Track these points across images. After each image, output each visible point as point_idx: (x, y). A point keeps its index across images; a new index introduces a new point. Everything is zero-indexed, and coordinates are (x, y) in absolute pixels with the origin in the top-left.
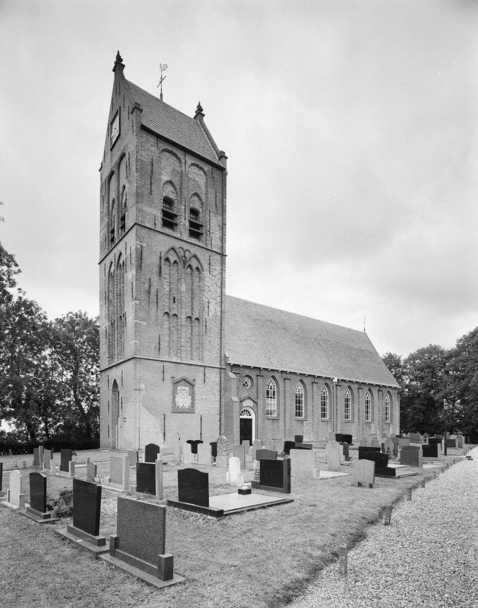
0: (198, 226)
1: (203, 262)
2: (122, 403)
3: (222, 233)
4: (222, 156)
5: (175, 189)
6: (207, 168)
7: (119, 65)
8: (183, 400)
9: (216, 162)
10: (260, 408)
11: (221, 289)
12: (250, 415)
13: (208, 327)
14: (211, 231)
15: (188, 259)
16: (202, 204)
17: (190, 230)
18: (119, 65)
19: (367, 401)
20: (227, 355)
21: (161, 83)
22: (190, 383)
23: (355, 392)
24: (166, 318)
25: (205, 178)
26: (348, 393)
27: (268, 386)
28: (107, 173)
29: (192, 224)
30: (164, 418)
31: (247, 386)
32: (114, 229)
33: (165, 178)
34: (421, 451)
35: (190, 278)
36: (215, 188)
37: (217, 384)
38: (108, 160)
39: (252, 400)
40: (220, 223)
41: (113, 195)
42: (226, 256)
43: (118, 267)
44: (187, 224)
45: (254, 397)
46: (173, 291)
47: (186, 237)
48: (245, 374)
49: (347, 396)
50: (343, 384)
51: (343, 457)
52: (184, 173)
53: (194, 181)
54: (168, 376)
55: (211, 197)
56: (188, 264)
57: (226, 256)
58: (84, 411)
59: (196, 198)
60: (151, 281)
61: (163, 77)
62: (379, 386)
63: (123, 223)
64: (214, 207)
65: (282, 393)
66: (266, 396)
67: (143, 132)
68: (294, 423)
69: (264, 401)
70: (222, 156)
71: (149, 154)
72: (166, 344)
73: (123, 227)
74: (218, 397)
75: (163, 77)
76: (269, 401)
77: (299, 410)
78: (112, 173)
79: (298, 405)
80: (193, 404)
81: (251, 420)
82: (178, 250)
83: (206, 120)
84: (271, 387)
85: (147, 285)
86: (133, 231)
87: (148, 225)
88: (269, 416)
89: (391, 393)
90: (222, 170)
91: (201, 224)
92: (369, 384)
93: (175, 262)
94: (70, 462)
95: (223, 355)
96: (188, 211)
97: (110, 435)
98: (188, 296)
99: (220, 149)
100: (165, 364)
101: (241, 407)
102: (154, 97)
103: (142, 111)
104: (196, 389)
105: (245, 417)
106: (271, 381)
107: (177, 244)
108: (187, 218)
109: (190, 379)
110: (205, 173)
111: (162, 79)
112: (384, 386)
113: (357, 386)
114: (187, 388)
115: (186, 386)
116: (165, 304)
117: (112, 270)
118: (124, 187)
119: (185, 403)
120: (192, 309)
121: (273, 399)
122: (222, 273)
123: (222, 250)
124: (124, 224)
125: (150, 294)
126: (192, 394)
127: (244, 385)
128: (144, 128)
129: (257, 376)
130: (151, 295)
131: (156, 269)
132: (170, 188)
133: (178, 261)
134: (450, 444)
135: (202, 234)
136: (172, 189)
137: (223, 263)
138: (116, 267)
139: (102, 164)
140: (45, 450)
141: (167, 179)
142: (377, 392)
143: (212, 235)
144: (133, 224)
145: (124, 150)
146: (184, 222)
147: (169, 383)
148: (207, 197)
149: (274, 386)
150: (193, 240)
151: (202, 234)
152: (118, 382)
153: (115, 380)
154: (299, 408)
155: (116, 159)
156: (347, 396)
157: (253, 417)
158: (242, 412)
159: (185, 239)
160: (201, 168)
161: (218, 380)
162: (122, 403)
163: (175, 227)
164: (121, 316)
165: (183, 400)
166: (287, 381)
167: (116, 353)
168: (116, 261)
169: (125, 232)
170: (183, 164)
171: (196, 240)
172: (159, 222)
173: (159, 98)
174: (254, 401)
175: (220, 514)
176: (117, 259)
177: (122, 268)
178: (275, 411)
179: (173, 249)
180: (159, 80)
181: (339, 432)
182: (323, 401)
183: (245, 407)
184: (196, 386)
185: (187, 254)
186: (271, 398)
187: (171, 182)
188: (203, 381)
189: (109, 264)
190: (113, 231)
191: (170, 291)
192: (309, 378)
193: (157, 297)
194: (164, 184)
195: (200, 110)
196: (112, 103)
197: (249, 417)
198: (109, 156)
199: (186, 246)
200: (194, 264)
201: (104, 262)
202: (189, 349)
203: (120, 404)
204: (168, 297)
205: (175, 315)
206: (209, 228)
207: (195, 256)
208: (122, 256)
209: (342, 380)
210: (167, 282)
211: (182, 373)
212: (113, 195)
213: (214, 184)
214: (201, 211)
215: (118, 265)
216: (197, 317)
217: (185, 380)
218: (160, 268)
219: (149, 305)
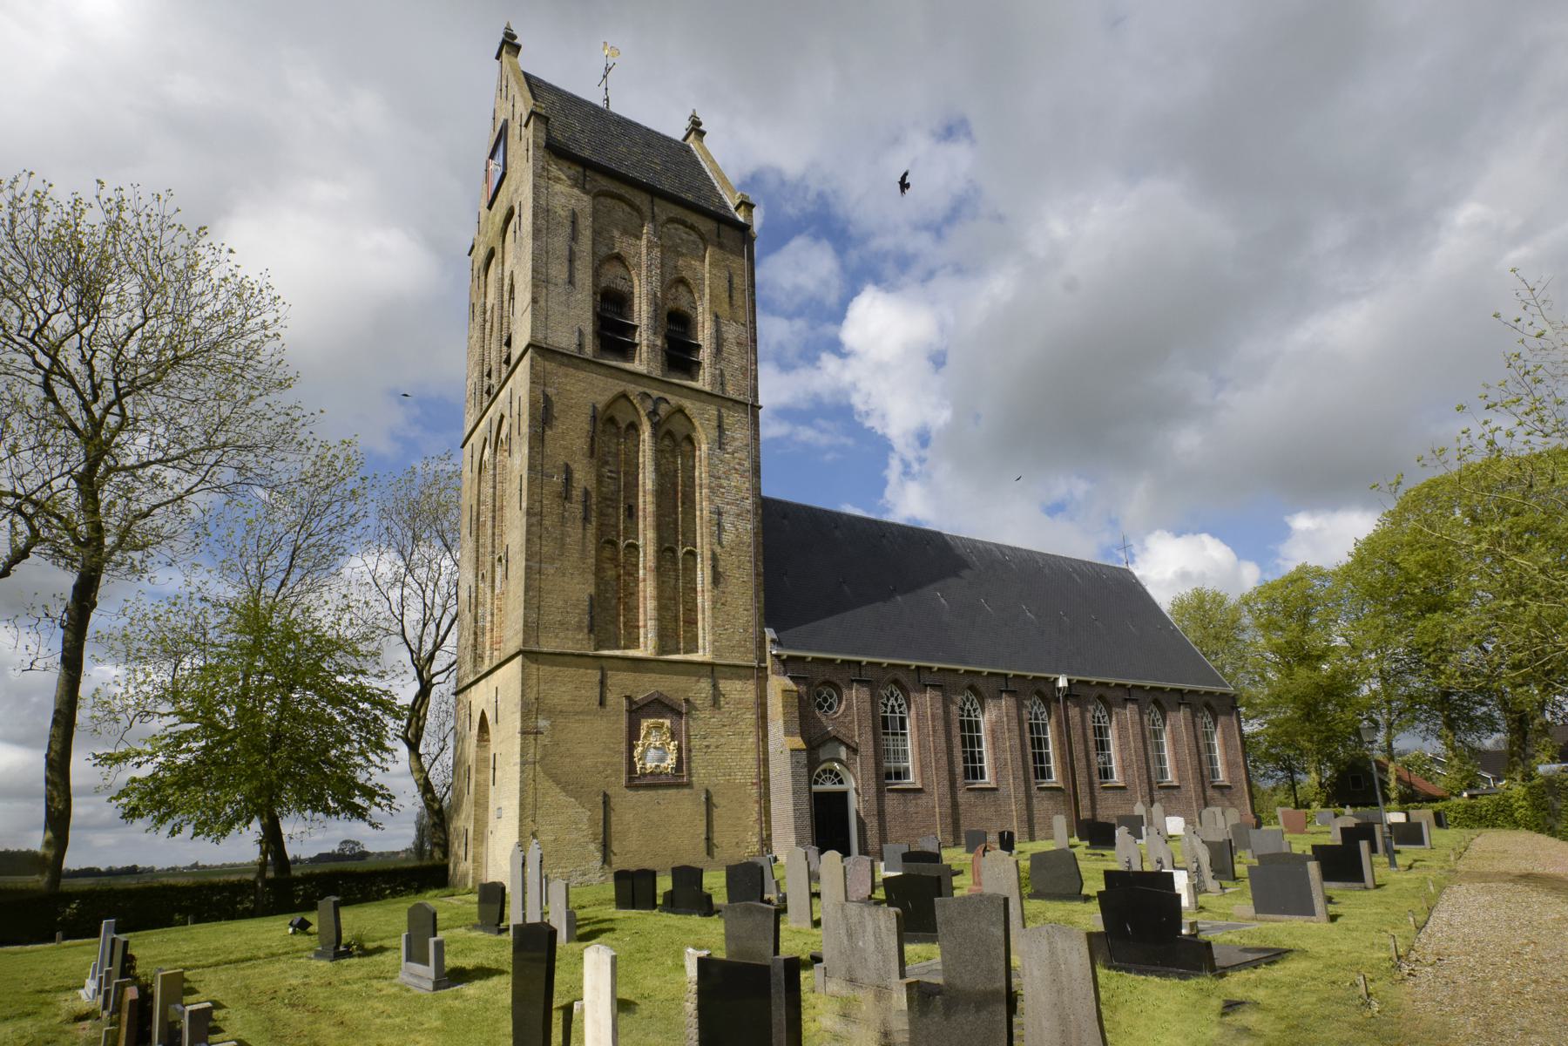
2: (494, 769)
12: (841, 782)
21: (605, 76)
27: (886, 706)
50: (1084, 691)
51: (686, 791)
56: (664, 429)
58: (1180, 927)
61: (610, 65)
64: (726, 306)
75: (610, 65)
81: (843, 796)
84: (893, 706)
86: (526, 361)
92: (1152, 688)
94: (432, 940)
105: (829, 787)
111: (608, 70)
140: (1102, 973)
160: (692, 227)
162: (494, 769)
180: (603, 72)
197: (838, 787)
219: (563, 525)
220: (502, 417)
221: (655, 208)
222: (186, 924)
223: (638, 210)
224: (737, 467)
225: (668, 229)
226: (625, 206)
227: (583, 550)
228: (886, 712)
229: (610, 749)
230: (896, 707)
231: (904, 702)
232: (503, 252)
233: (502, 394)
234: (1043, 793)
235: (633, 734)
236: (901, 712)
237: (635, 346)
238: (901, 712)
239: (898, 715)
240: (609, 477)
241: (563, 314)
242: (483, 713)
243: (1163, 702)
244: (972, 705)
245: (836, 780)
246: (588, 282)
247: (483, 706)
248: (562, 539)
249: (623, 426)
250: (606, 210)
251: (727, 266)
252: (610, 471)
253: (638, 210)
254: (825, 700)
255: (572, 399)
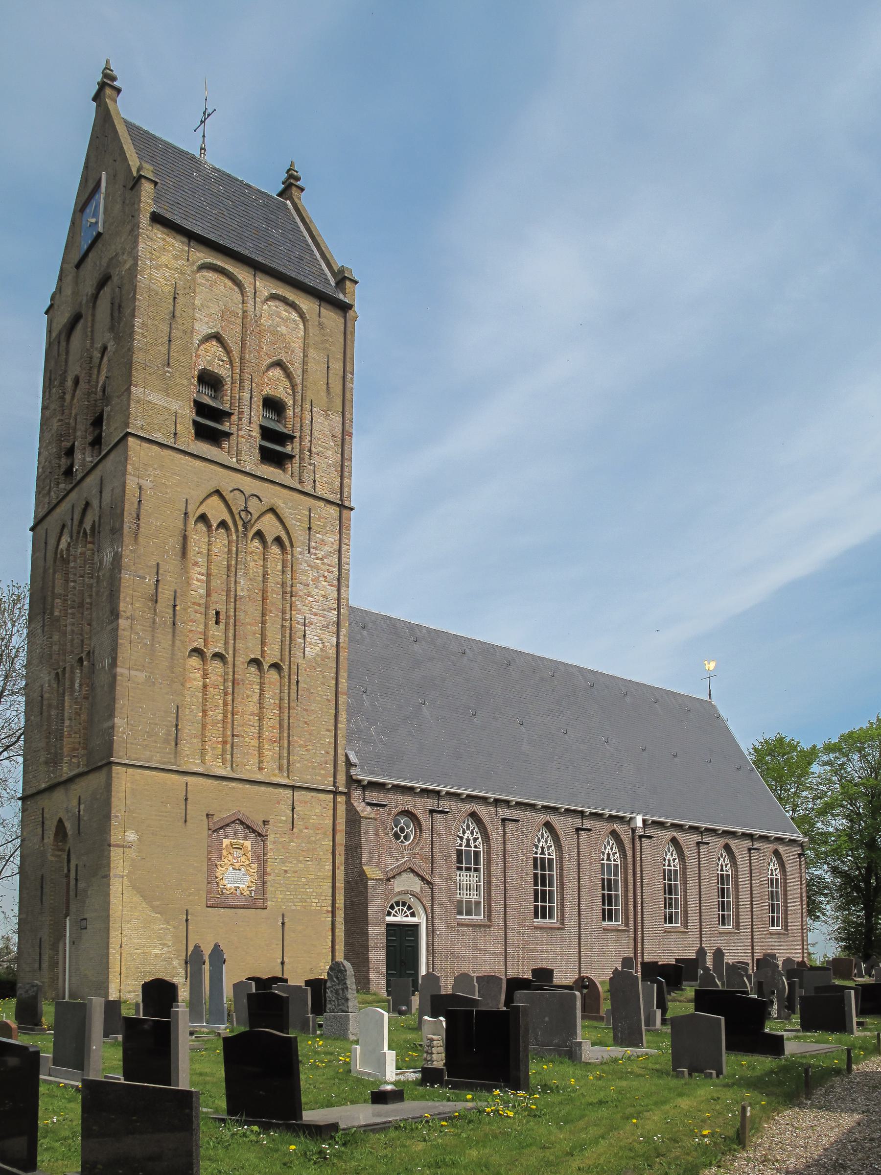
0: (283, 438)
1: (291, 522)
2: (76, 880)
3: (342, 455)
4: (342, 279)
5: (228, 351)
11: (339, 590)
12: (413, 915)
14: (313, 450)
15: (255, 516)
16: (293, 387)
17: (262, 449)
19: (722, 875)
21: (203, 122)
22: (254, 831)
23: (690, 853)
25: (301, 326)
26: (546, 842)
27: (461, 838)
28: (63, 318)
29: (267, 433)
30: (187, 920)
31: (406, 838)
33: (203, 328)
36: (325, 349)
37: (325, 833)
38: (68, 291)
39: (418, 875)
40: (338, 431)
42: (352, 509)
43: (78, 537)
44: (256, 433)
45: (424, 868)
46: (214, 597)
47: (251, 460)
48: (400, 808)
49: (722, 870)
52: (251, 313)
53: (275, 333)
54: (196, 813)
55: (316, 369)
57: (352, 509)
59: (277, 372)
60: (161, 572)
61: (209, 111)
63: (97, 432)
64: (323, 394)
65: (497, 859)
66: (455, 865)
69: (450, 876)
71: (167, 275)
72: (196, 729)
73: (97, 442)
74: (329, 867)
75: (209, 111)
76: (464, 878)
78: (77, 318)
79: (606, 892)
80: (262, 884)
81: (415, 927)
82: (229, 497)
83: (305, 200)
84: (468, 840)
85: (150, 580)
87: (158, 437)
91: (291, 433)
96: (258, 402)
97: (45, 965)
99: (339, 262)
100: (189, 779)
104: (269, 846)
106: (468, 827)
107: (228, 481)
108: (254, 419)
109: (256, 820)
110: (302, 315)
111: (206, 115)
112: (764, 838)
114: (248, 844)
115: (245, 838)
117: (63, 545)
118: (104, 349)
119: (242, 882)
120: (263, 643)
121: (473, 873)
123: (341, 494)
125: (156, 602)
130: (158, 604)
131: (174, 543)
135: (291, 457)
136: (220, 351)
137: (342, 527)
138: (75, 535)
139: (52, 298)
141: (210, 331)
142: (746, 852)
143: (316, 459)
145: (108, 266)
147: (199, 827)
148: (304, 371)
149: (475, 840)
151: (291, 457)
152: (68, 825)
154: (541, 896)
155: (88, 288)
156: (722, 870)
157: (421, 919)
158: (392, 907)
159: (248, 469)
160: (293, 306)
162: (76, 880)
166: (510, 826)
167: (66, 750)
168: (76, 522)
169: (100, 453)
171: (278, 471)
172: (186, 430)
174: (423, 879)
176: (77, 517)
177: (89, 539)
178: (478, 903)
179: (218, 492)
182: (770, 889)
183: (399, 893)
184: (270, 839)
185: (253, 504)
186: (468, 869)
187: (217, 337)
188: (290, 826)
190: (70, 452)
191: (208, 595)
193: (174, 611)
198: (69, 279)
200: (269, 526)
203: (72, 882)
204: (203, 610)
206: (311, 441)
207: (272, 510)
210: (200, 574)
213: (323, 342)
214: (290, 402)
216: (276, 660)
217: (242, 823)
218: (185, 538)
220: (87, 505)
221: (257, 283)
224: (326, 574)
225: (269, 307)
226: (226, 281)
227: (172, 659)
228: (461, 845)
230: (472, 841)
232: (93, 321)
233: (89, 480)
236: (475, 847)
239: (473, 849)
242: (60, 821)
243: (733, 847)
245: (408, 913)
247: (62, 814)
248: (152, 645)
249: (215, 525)
250: (208, 284)
251: (325, 349)
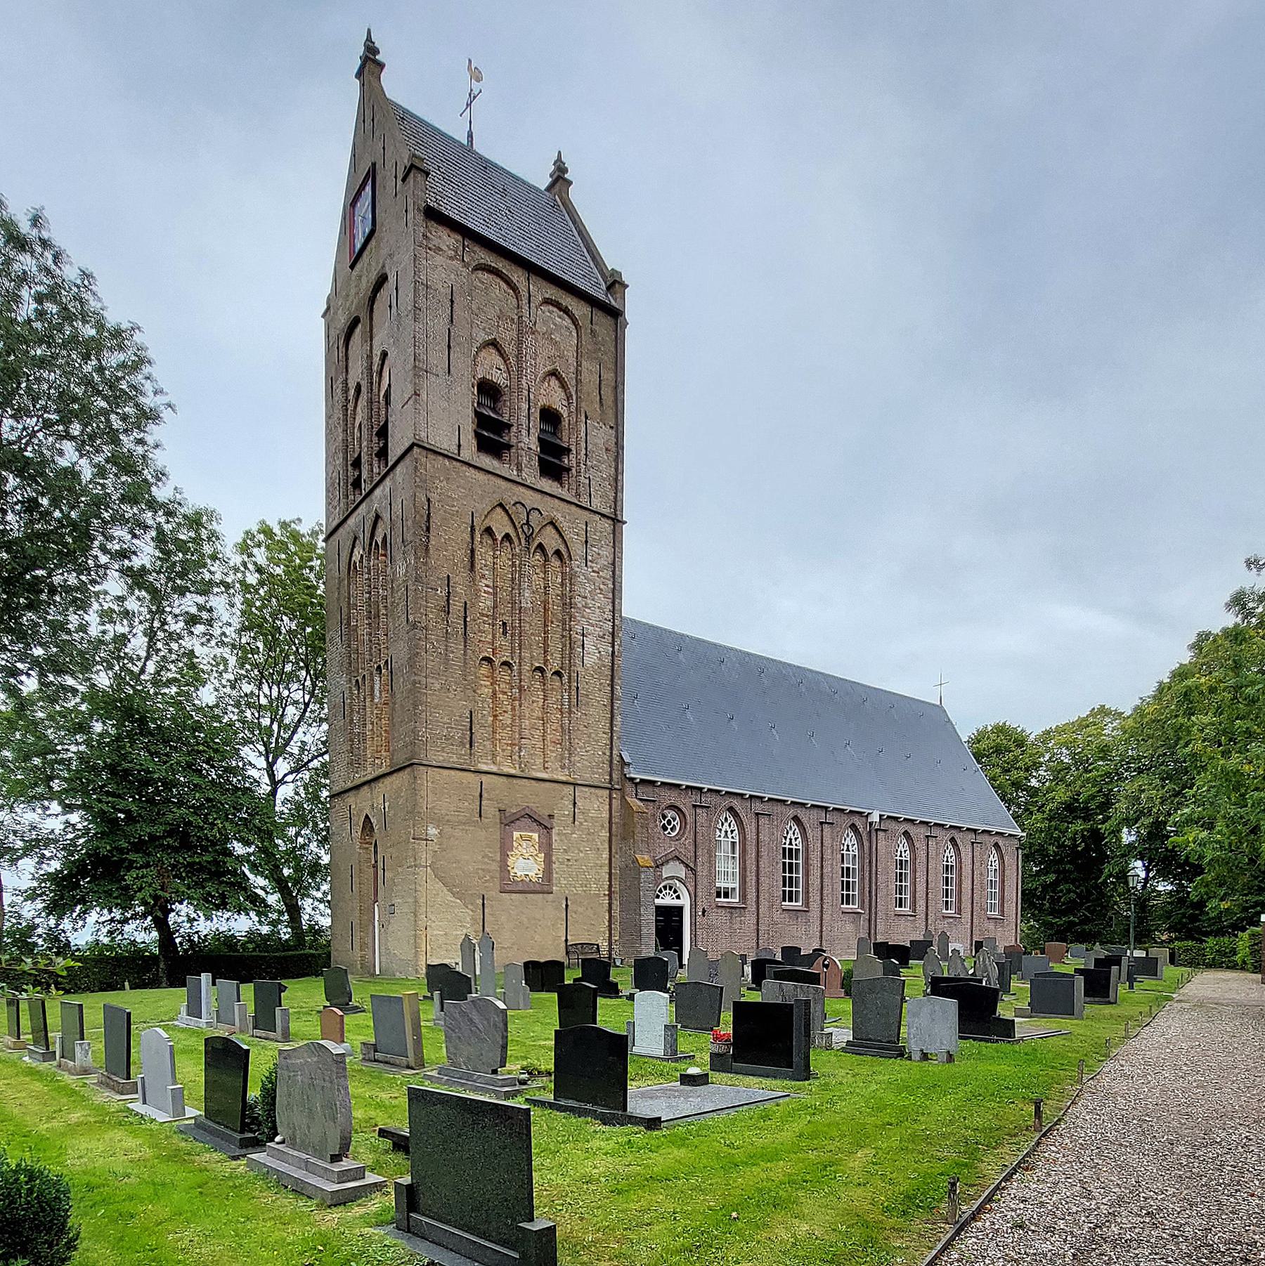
5: (505, 359)
6: (580, 309)
7: (371, 63)
8: (525, 864)
9: (602, 297)
10: (703, 882)
12: (678, 897)
13: (581, 691)
16: (569, 397)
18: (371, 63)
20: (627, 759)
21: (469, 105)
24: (485, 670)
28: (342, 320)
32: (360, 455)
34: (1080, 981)
35: (542, 575)
41: (357, 373)
43: (370, 549)
44: (535, 446)
45: (686, 852)
46: (501, 610)
50: (892, 825)
62: (975, 831)
63: (357, 473)
64: (597, 406)
67: (432, 224)
68: (777, 916)
70: (615, 282)
73: (383, 453)
77: (791, 886)
78: (355, 322)
81: (679, 910)
83: (574, 194)
84: (791, 839)
88: (722, 899)
89: (1003, 848)
90: (615, 314)
91: (565, 445)
93: (507, 537)
95: (616, 759)
98: (537, 621)
100: (484, 778)
101: (659, 879)
102: (454, 141)
103: (427, 174)
105: (667, 900)
106: (726, 819)
107: (513, 494)
111: (472, 97)
113: (923, 831)
114: (536, 836)
115: (532, 831)
116: (485, 638)
117: (356, 557)
118: (384, 355)
122: (614, 564)
123: (615, 510)
124: (386, 445)
125: (448, 613)
126: (547, 848)
127: (665, 828)
128: (433, 215)
129: (695, 806)
131: (462, 555)
132: (491, 357)
133: (513, 535)
134: (1149, 967)
136: (498, 360)
144: (407, 445)
146: (527, 440)
150: (547, 485)
153: (367, 816)
155: (366, 284)
157: (685, 901)
158: (661, 891)
160: (566, 311)
161: (606, 815)
163: (506, 455)
164: (379, 667)
165: (525, 864)
168: (368, 535)
169: (387, 465)
170: (525, 301)
173: (466, 143)
174: (687, 866)
175: (653, 1123)
178: (733, 889)
179: (501, 505)
181: (880, 939)
189: (349, 543)
190: (357, 464)
191: (495, 607)
192: (815, 811)
194: (479, 349)
195: (560, 178)
196: (354, 155)
197: (676, 902)
199: (530, 499)
200: (550, 540)
201: (335, 537)
202: (540, 745)
205: (505, 663)
208: (380, 523)
209: (889, 817)
211: (526, 796)
212: (357, 373)
215: (371, 544)
217: (530, 817)
218: (473, 551)
222: (123, 988)
223: (514, 288)
226: (502, 283)
228: (785, 844)
229: (489, 858)
230: (729, 833)
231: (736, 828)
234: (847, 917)
235: (505, 848)
237: (568, 470)
238: (732, 837)
240: (485, 592)
241: (444, 410)
244: (794, 834)
246: (467, 373)
252: (487, 586)
253: (514, 288)
254: (669, 822)
255: (453, 506)
